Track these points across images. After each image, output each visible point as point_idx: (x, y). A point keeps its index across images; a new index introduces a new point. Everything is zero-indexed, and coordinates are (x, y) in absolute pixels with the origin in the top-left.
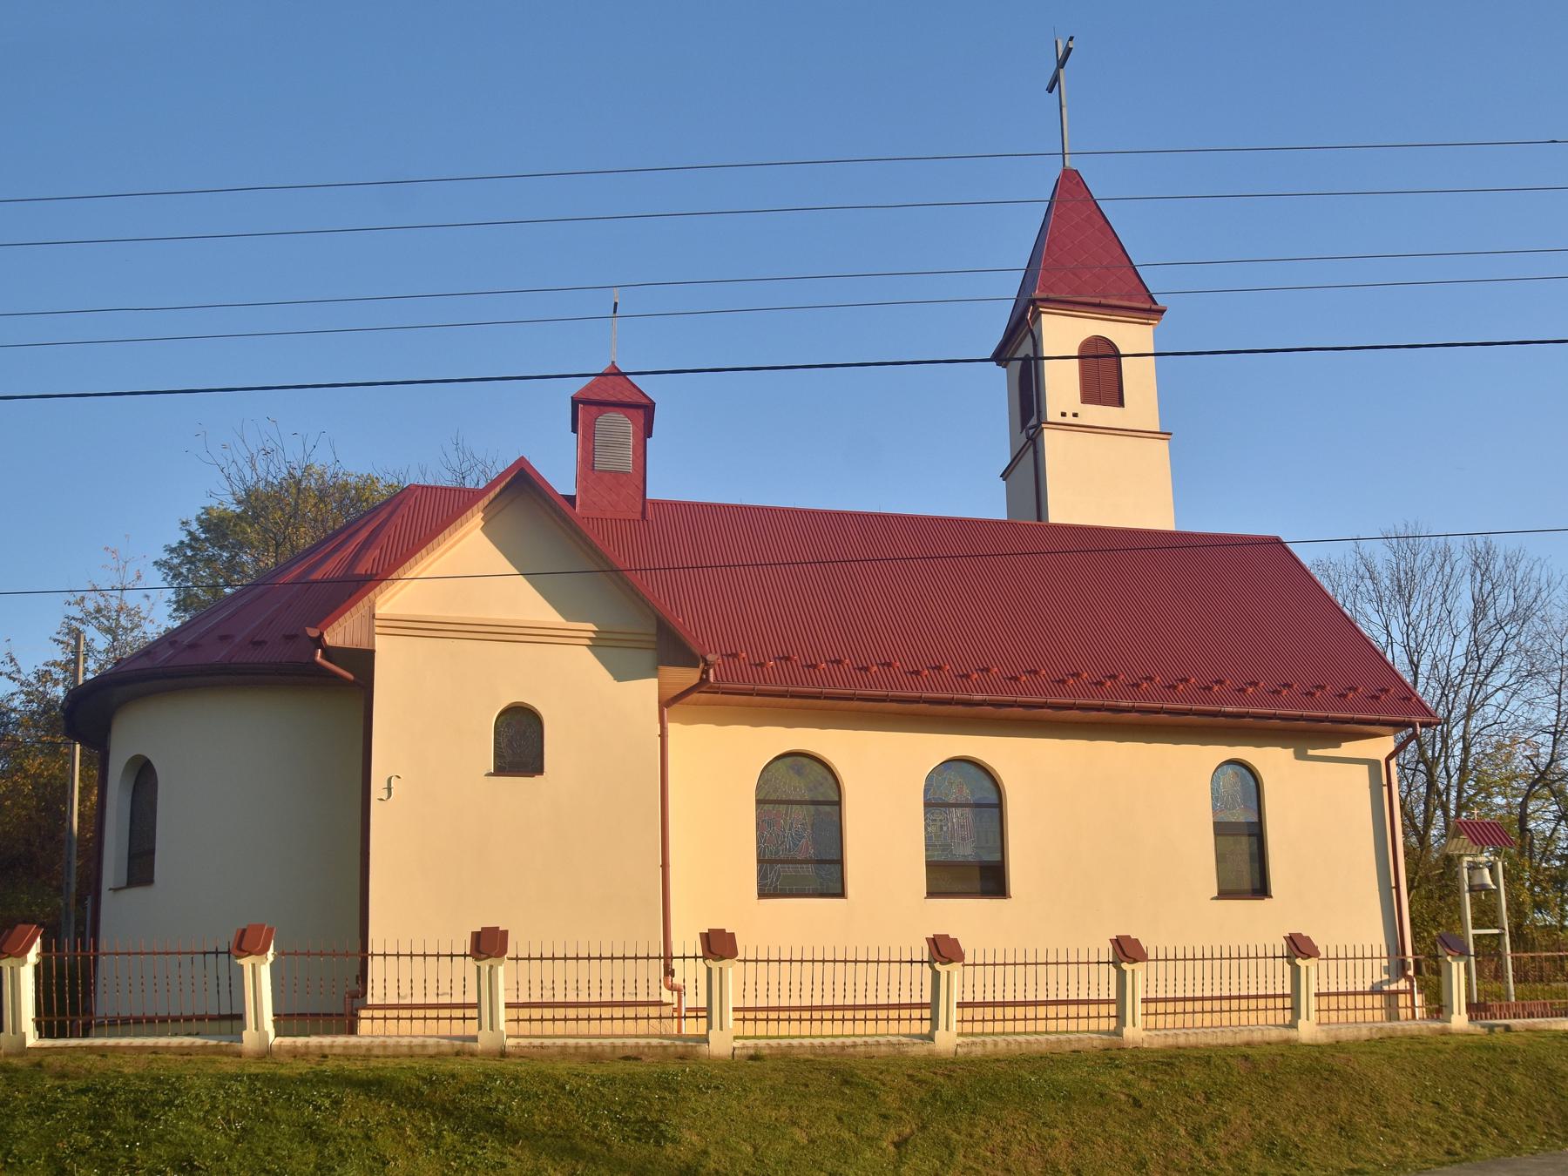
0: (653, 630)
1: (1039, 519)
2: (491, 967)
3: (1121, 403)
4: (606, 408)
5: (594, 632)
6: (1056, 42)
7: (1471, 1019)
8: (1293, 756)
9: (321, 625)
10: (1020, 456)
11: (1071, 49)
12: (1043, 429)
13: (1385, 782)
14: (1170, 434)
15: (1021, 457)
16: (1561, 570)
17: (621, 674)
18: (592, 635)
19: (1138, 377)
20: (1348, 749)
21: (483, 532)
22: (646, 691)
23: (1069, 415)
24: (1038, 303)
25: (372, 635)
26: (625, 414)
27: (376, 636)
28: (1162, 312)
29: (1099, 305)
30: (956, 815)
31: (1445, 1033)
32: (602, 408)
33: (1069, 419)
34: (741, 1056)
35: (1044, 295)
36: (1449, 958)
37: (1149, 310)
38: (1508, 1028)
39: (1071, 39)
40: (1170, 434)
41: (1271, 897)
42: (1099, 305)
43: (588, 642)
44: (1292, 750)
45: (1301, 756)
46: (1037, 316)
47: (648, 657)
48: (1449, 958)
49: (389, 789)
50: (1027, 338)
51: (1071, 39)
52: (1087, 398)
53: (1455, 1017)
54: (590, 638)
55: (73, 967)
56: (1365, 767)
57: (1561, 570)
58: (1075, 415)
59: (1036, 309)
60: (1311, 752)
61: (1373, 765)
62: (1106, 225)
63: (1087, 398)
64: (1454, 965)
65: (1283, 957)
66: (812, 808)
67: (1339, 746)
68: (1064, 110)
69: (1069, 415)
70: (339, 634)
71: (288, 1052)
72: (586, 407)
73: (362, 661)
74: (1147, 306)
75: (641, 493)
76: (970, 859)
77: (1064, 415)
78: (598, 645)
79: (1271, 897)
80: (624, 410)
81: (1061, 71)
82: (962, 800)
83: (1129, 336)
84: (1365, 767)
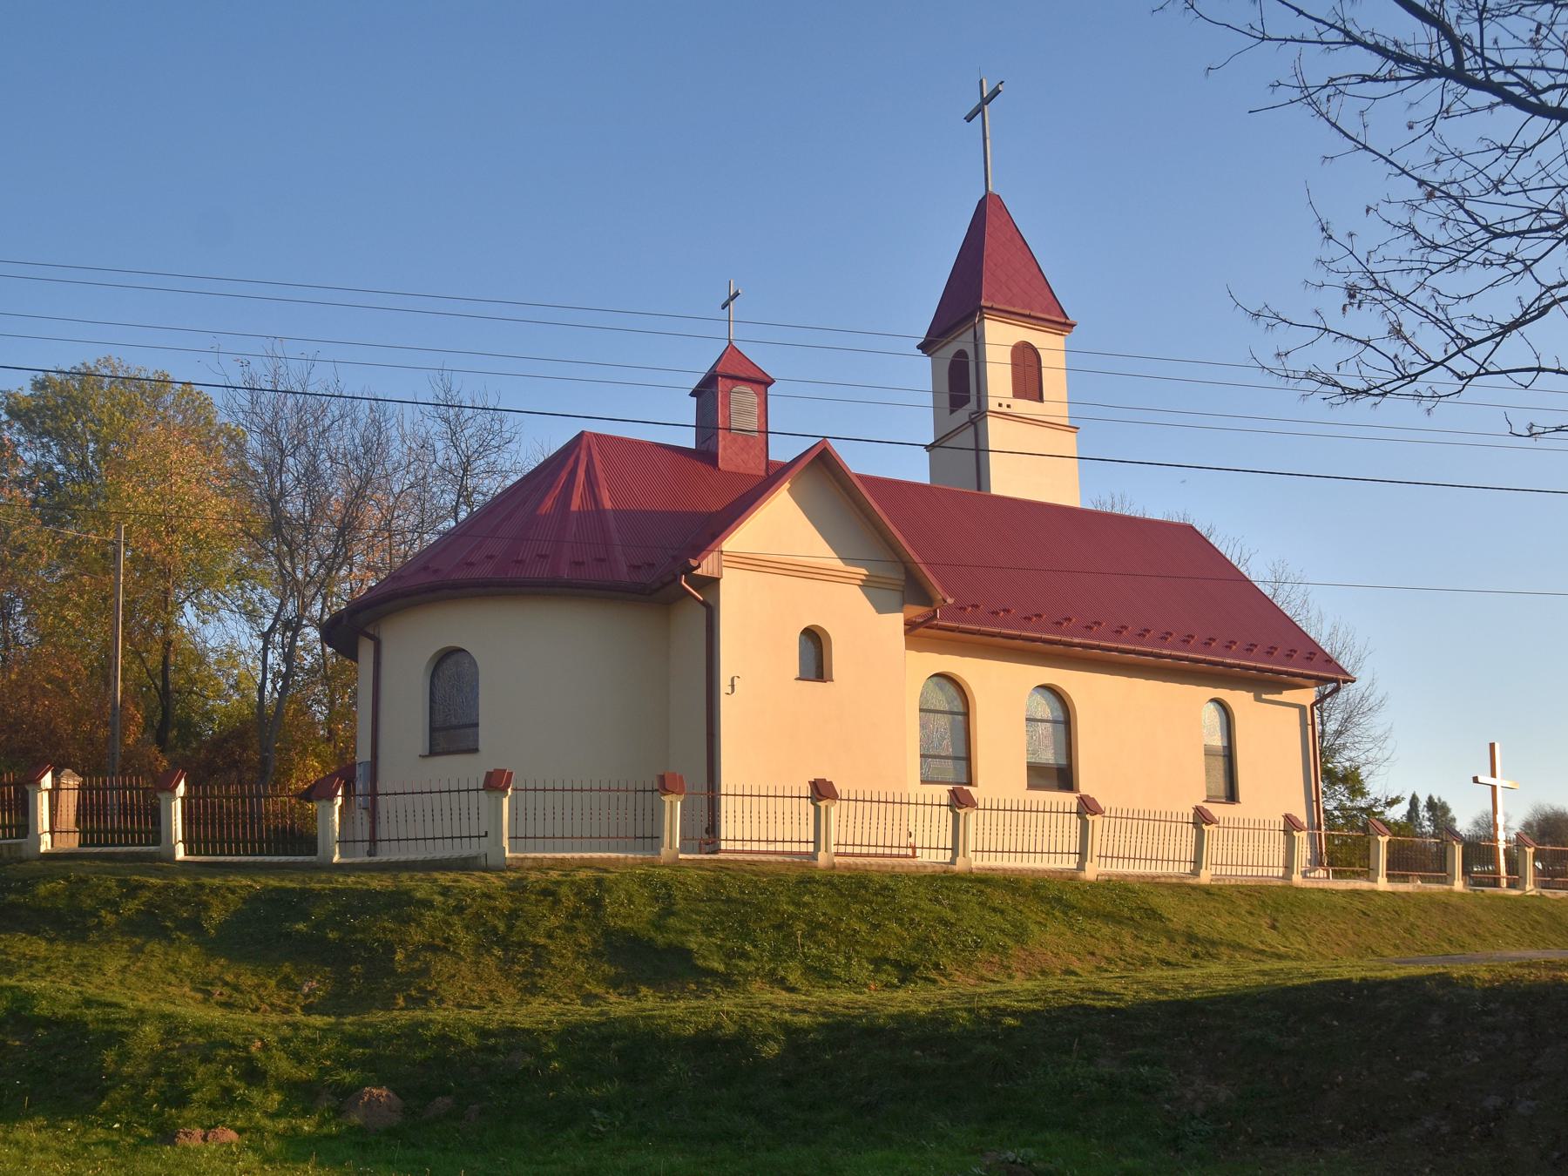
0: (903, 577)
1: (979, 489)
2: (966, 814)
3: (1040, 399)
4: (738, 382)
5: (865, 575)
6: (981, 81)
7: (1464, 886)
8: (1253, 698)
9: (699, 557)
10: (958, 431)
11: (1000, 91)
12: (987, 416)
13: (1310, 722)
14: (1077, 428)
15: (957, 434)
16: (1249, 549)
17: (881, 608)
18: (864, 578)
19: (1054, 380)
20: (1288, 696)
21: (789, 493)
22: (896, 621)
23: (1004, 406)
24: (984, 310)
25: (720, 567)
26: (753, 390)
27: (724, 568)
28: (1072, 326)
29: (1029, 316)
30: (1041, 727)
31: (1451, 892)
32: (734, 381)
33: (1004, 409)
34: (1101, 880)
35: (989, 305)
36: (1454, 843)
37: (1063, 324)
38: (1483, 891)
39: (1002, 83)
40: (1077, 428)
41: (1239, 802)
42: (1029, 316)
43: (859, 585)
44: (1252, 694)
45: (1258, 699)
46: (982, 319)
47: (896, 597)
48: (1454, 843)
49: (733, 686)
50: (968, 332)
51: (1002, 83)
52: (1017, 395)
53: (1456, 882)
54: (861, 580)
55: (244, 814)
56: (1297, 710)
57: (1249, 549)
58: (1008, 406)
59: (982, 313)
60: (1264, 696)
61: (1302, 708)
62: (1025, 246)
63: (1017, 395)
64: (1457, 846)
65: (1075, 853)
66: (950, 716)
67: (1281, 693)
68: (988, 141)
69: (1004, 406)
70: (706, 567)
71: (845, 868)
72: (724, 379)
73: (712, 583)
74: (1063, 320)
75: (764, 455)
76: (1051, 762)
77: (1000, 405)
78: (867, 586)
79: (1239, 802)
80: (751, 384)
81: (986, 106)
82: (1045, 717)
83: (1047, 343)
84: (1297, 710)
